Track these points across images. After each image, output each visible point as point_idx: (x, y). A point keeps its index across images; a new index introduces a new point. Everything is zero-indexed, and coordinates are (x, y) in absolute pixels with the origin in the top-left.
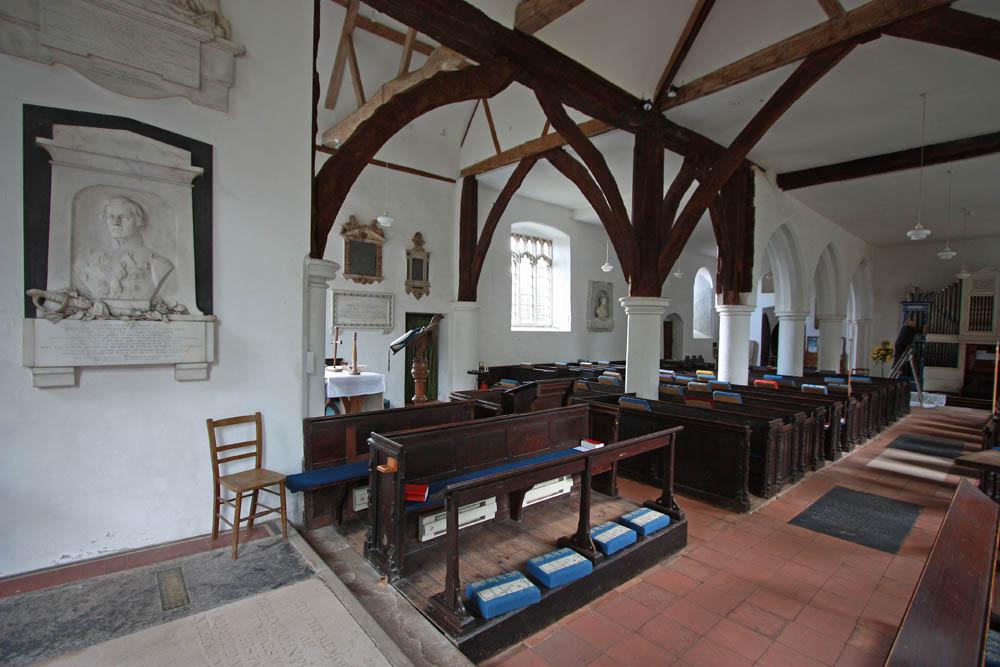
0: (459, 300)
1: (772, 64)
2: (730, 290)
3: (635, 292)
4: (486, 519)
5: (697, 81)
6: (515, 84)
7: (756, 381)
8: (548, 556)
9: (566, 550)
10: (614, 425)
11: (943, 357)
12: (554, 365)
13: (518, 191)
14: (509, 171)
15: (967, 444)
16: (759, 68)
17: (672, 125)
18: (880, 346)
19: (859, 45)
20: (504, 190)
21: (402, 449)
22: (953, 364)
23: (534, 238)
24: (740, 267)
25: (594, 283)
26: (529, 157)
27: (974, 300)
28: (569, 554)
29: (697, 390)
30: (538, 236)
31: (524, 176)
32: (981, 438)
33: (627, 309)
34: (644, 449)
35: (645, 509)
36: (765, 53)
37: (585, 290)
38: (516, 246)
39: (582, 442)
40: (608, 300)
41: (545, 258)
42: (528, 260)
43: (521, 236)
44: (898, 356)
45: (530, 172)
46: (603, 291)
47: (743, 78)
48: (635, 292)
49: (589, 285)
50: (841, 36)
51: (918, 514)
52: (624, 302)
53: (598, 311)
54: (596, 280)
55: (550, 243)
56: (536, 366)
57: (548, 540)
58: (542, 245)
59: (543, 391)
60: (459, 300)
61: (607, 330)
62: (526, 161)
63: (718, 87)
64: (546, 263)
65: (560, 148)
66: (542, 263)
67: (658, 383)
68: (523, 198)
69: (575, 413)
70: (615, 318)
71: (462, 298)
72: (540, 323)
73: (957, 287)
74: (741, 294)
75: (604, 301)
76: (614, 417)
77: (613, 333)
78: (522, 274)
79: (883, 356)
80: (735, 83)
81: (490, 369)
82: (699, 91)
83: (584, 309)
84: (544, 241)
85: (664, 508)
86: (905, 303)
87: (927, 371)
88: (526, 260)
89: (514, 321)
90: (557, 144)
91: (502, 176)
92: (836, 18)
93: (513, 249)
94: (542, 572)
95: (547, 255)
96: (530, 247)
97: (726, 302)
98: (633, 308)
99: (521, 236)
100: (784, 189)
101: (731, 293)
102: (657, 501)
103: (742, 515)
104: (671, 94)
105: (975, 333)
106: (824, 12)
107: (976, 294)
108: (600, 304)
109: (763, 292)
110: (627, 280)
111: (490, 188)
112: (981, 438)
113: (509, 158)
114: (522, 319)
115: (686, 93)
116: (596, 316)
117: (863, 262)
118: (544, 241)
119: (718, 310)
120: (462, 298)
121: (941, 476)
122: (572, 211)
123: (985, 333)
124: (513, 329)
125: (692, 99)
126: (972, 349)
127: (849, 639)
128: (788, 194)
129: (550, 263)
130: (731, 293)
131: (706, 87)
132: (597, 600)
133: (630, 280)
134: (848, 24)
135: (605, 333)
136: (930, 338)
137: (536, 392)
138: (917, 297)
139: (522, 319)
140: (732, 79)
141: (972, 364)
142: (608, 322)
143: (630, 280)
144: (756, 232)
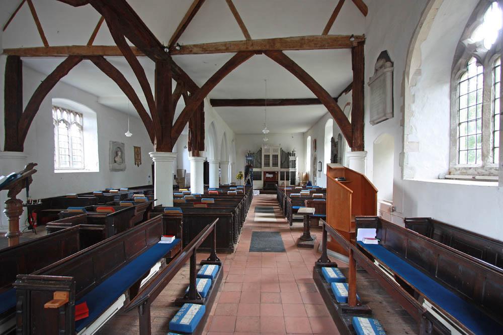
0: (5, 150)
1: (224, 50)
2: (196, 149)
3: (158, 149)
4: (119, 309)
5: (190, 46)
6: (89, 4)
7: (314, 194)
8: (179, 314)
9: (186, 305)
10: (114, 224)
11: (257, 177)
12: (92, 193)
13: (63, 79)
14: (54, 63)
15: (274, 207)
16: (219, 50)
17: (174, 63)
18: (239, 174)
19: (255, 55)
20: (203, 86)
21: (73, 280)
22: (260, 179)
23: (69, 111)
24: (199, 139)
25: (114, 142)
26: (76, 56)
27: (265, 155)
28: (189, 307)
29: (189, 199)
30: (65, 108)
31: (71, 68)
32: (277, 204)
33: (154, 158)
34: (208, 234)
35: (205, 266)
36: (225, 44)
37: (107, 147)
38: (57, 115)
39: (162, 238)
40: (122, 153)
41: (78, 125)
42: (65, 124)
43: (72, 112)
44: (246, 177)
45: (76, 66)
46: (119, 147)
47: (211, 52)
48: (158, 149)
49: (110, 144)
50: (251, 48)
51: (280, 235)
52: (153, 155)
53: (116, 159)
54: (114, 141)
55: (81, 115)
56: (79, 195)
57: (166, 304)
58: (75, 116)
59: (138, 211)
60: (5, 150)
61: (122, 170)
62: (73, 58)
63: (200, 52)
64: (78, 128)
65: (102, 56)
66: (74, 128)
67: (173, 198)
68: (65, 83)
69: (157, 221)
70: (126, 163)
71: (8, 148)
72: (75, 167)
73: (260, 151)
74: (200, 152)
75: (119, 154)
76: (180, 219)
77: (125, 172)
78: (61, 134)
79: (240, 177)
80: (208, 53)
81: (43, 200)
82: (191, 51)
83: (107, 159)
84: (77, 113)
85: (212, 262)
86: (246, 156)
87: (254, 181)
88: (62, 125)
89: (56, 166)
90: (101, 54)
91: (51, 64)
92: (249, 40)
93: (55, 117)
94: (183, 326)
95: (79, 122)
96: (70, 118)
97: (193, 155)
98: (158, 159)
99: (58, 108)
100: (213, 106)
101: (196, 151)
102: (208, 259)
103: (232, 254)
104: (178, 48)
105: (266, 168)
106: (244, 36)
107: (273, 154)
108: (117, 155)
109: (278, 155)
110: (153, 143)
111: (37, 71)
112: (277, 204)
113: (58, 53)
114: (62, 164)
115: (184, 50)
116: (115, 162)
117: (233, 141)
118: (77, 113)
119: (189, 159)
120: (8, 148)
121: (275, 220)
122: (98, 97)
123: (268, 168)
124: (56, 171)
125: (188, 54)
126: (265, 173)
127: (299, 290)
128: (213, 108)
129: (82, 128)
130: (196, 151)
131: (195, 50)
132: (206, 325)
133: (155, 142)
134: (252, 45)
135: (121, 172)
136: (255, 170)
137: (134, 212)
138: (250, 155)
139: (62, 164)
140: (207, 51)
141: (265, 178)
142: (122, 166)
143: (155, 142)
144: (205, 124)
